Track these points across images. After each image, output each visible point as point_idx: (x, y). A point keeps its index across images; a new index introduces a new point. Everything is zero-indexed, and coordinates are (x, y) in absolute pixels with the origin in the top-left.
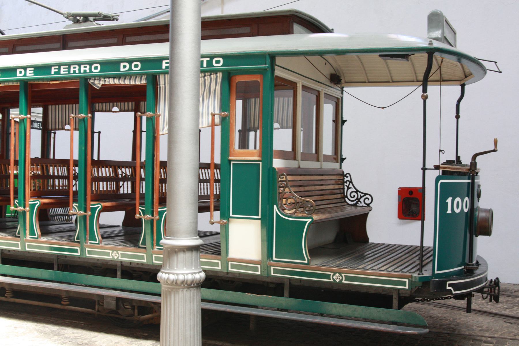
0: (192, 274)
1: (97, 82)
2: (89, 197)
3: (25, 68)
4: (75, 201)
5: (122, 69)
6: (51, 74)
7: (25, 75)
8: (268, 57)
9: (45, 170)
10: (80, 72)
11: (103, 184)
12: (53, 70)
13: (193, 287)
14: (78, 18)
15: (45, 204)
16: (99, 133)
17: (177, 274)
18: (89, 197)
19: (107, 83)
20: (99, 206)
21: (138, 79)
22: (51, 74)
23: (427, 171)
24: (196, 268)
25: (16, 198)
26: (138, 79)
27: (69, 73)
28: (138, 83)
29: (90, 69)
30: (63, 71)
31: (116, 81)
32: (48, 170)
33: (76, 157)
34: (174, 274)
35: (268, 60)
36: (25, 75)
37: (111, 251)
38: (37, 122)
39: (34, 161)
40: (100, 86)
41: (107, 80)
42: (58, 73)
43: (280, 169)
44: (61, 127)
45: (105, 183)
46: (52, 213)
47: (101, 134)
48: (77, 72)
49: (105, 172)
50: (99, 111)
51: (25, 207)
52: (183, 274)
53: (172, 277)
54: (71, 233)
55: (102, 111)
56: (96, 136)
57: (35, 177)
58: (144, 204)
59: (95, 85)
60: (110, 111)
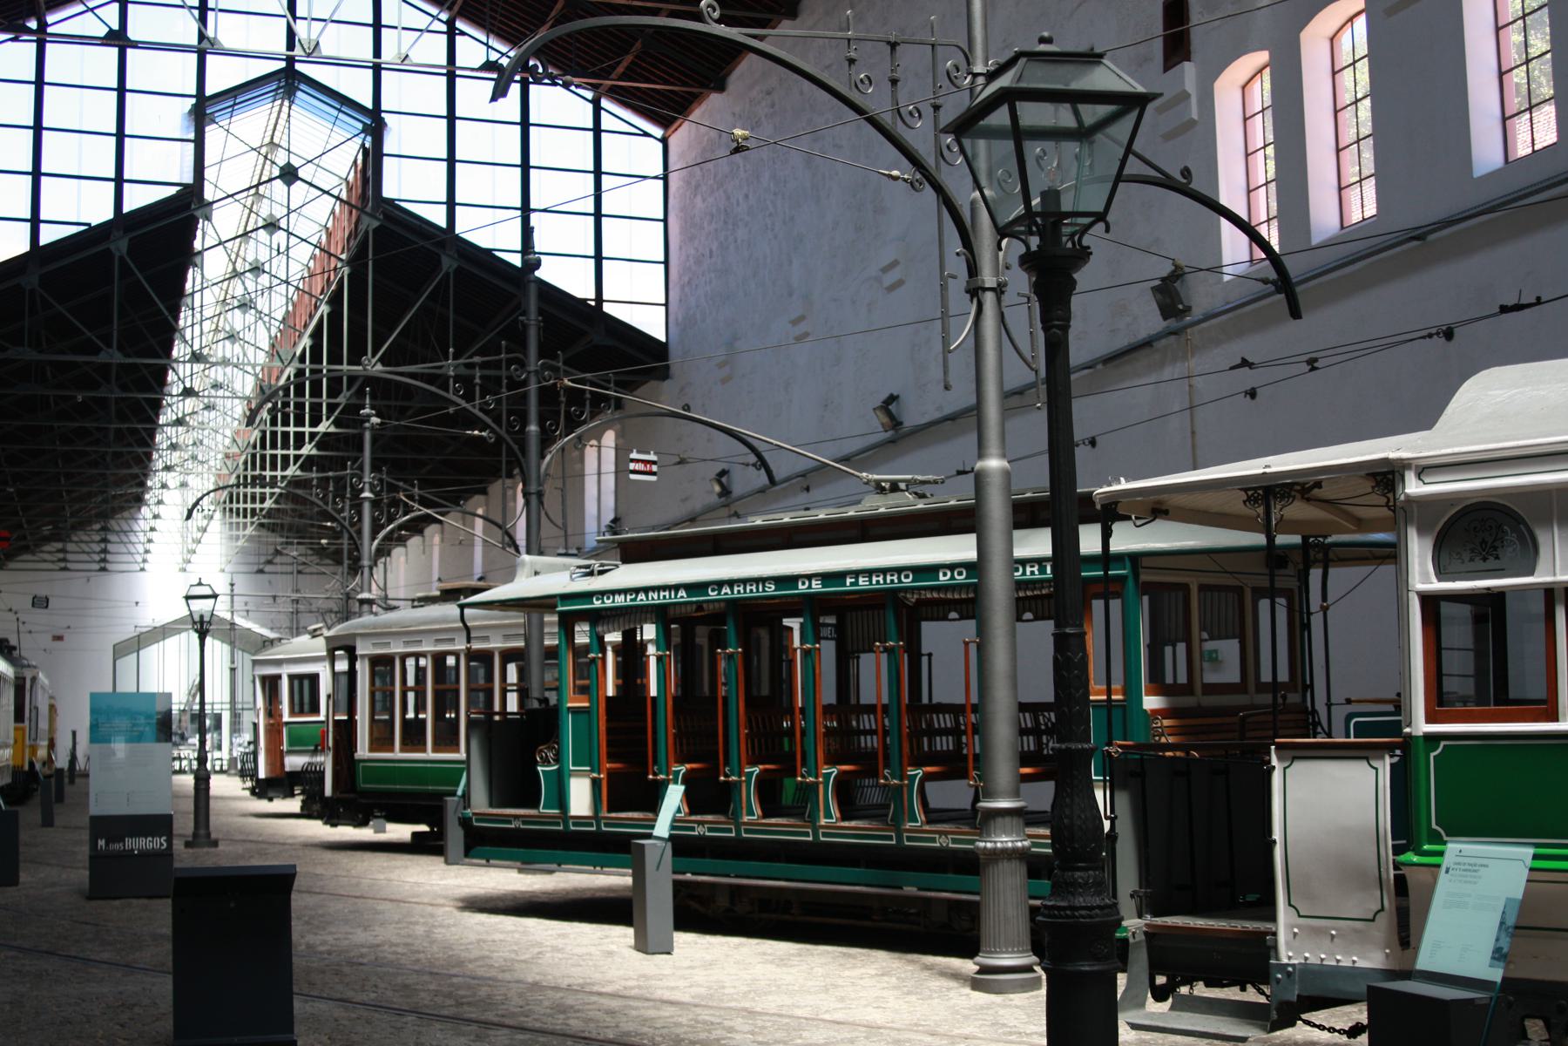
0: (1012, 842)
1: (908, 596)
2: (905, 760)
3: (809, 577)
4: (887, 766)
5: (941, 578)
6: (845, 586)
7: (810, 587)
8: (1127, 559)
9: (844, 722)
10: (885, 583)
11: (941, 740)
12: (849, 581)
13: (1015, 859)
14: (883, 484)
15: (845, 772)
16: (930, 655)
17: (995, 842)
18: (905, 760)
19: (923, 597)
20: (920, 772)
21: (964, 591)
22: (845, 586)
23: (1333, 708)
24: (1018, 835)
25: (804, 764)
26: (964, 591)
27: (871, 584)
28: (964, 596)
29: (899, 578)
30: (863, 582)
31: (935, 595)
32: (848, 722)
33: (885, 700)
34: (991, 842)
35: (1128, 564)
36: (810, 587)
37: (937, 836)
38: (828, 625)
39: (828, 709)
40: (913, 600)
41: (923, 592)
42: (856, 583)
43: (1155, 712)
44: (867, 648)
45: (944, 738)
46: (862, 803)
47: (933, 658)
48: (882, 582)
49: (946, 721)
50: (927, 619)
51: (817, 777)
52: (1002, 842)
53: (989, 845)
54: (883, 812)
55: (932, 619)
56: (925, 660)
57: (829, 732)
58: (189, 551)
59: (907, 599)
60: (945, 618)
